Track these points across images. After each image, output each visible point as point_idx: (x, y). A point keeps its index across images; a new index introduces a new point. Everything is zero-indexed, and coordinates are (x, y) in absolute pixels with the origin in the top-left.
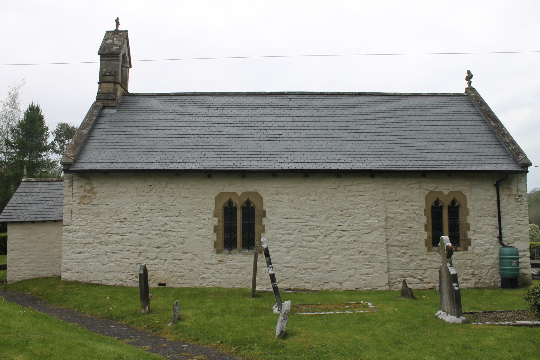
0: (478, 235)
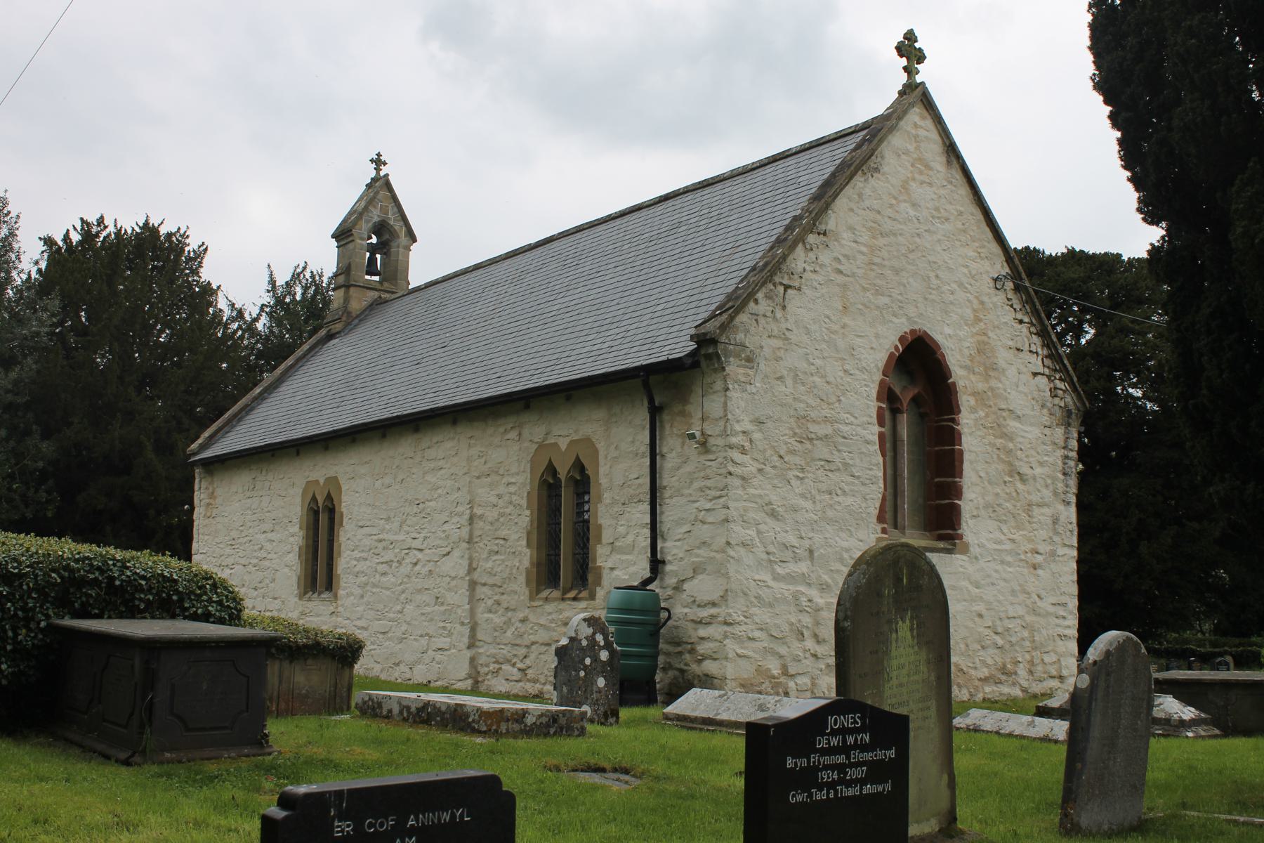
0: (619, 556)
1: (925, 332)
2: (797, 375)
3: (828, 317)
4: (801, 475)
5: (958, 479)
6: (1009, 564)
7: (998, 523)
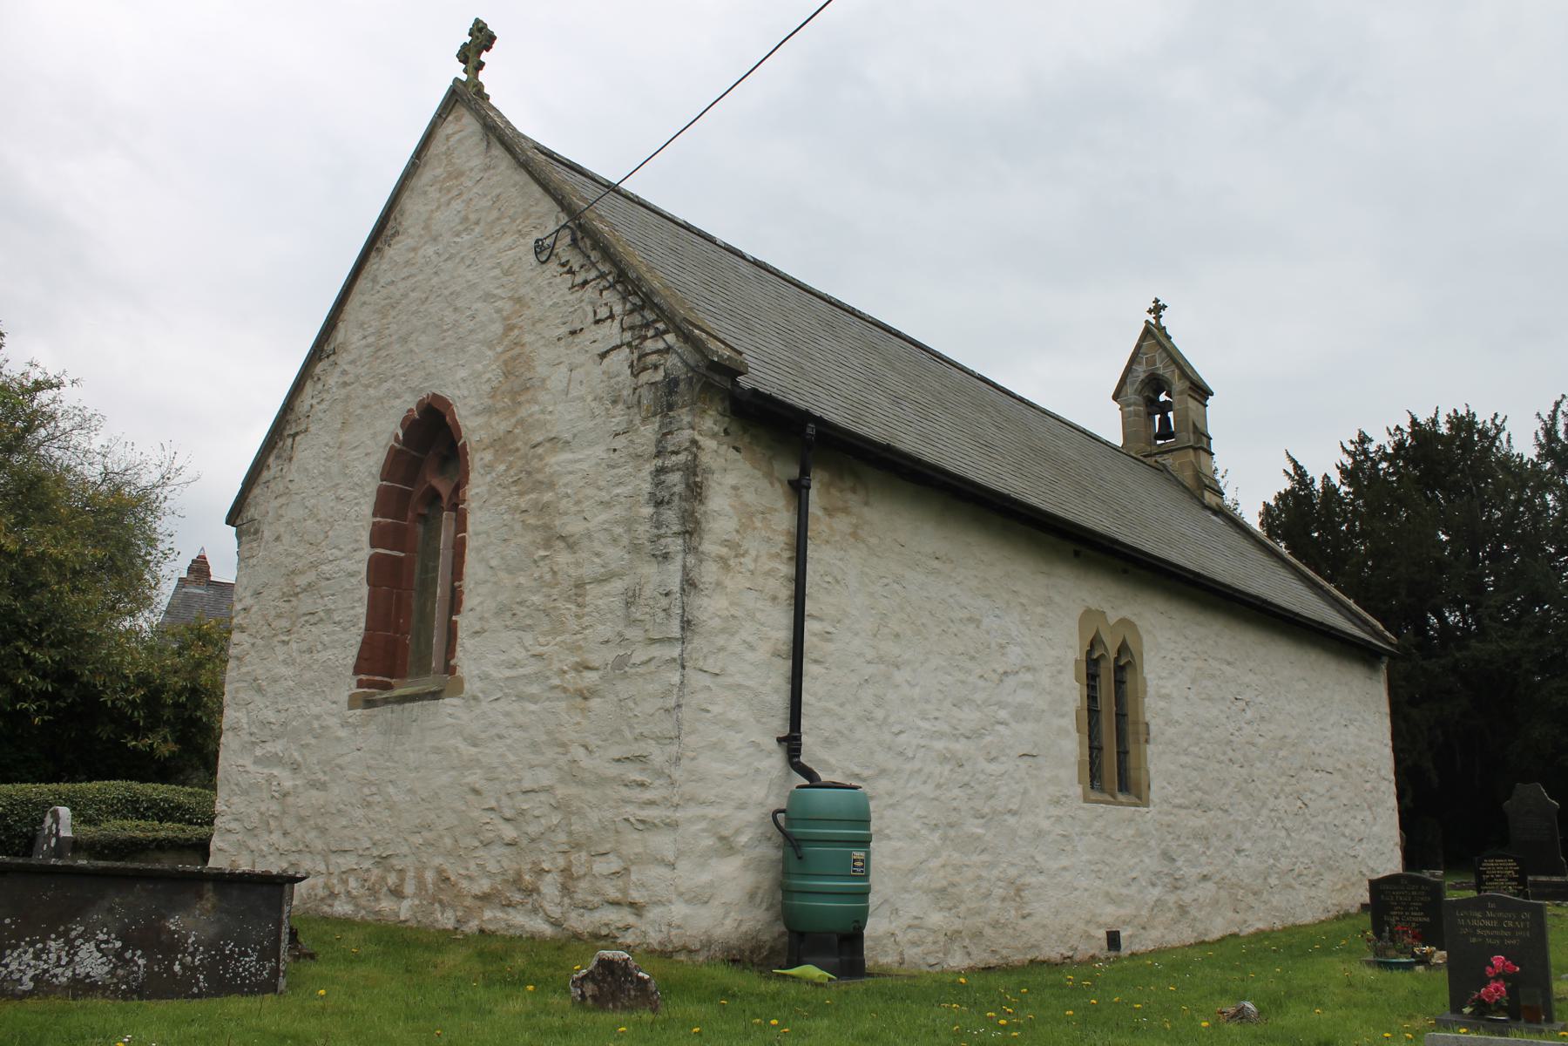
6: (533, 699)
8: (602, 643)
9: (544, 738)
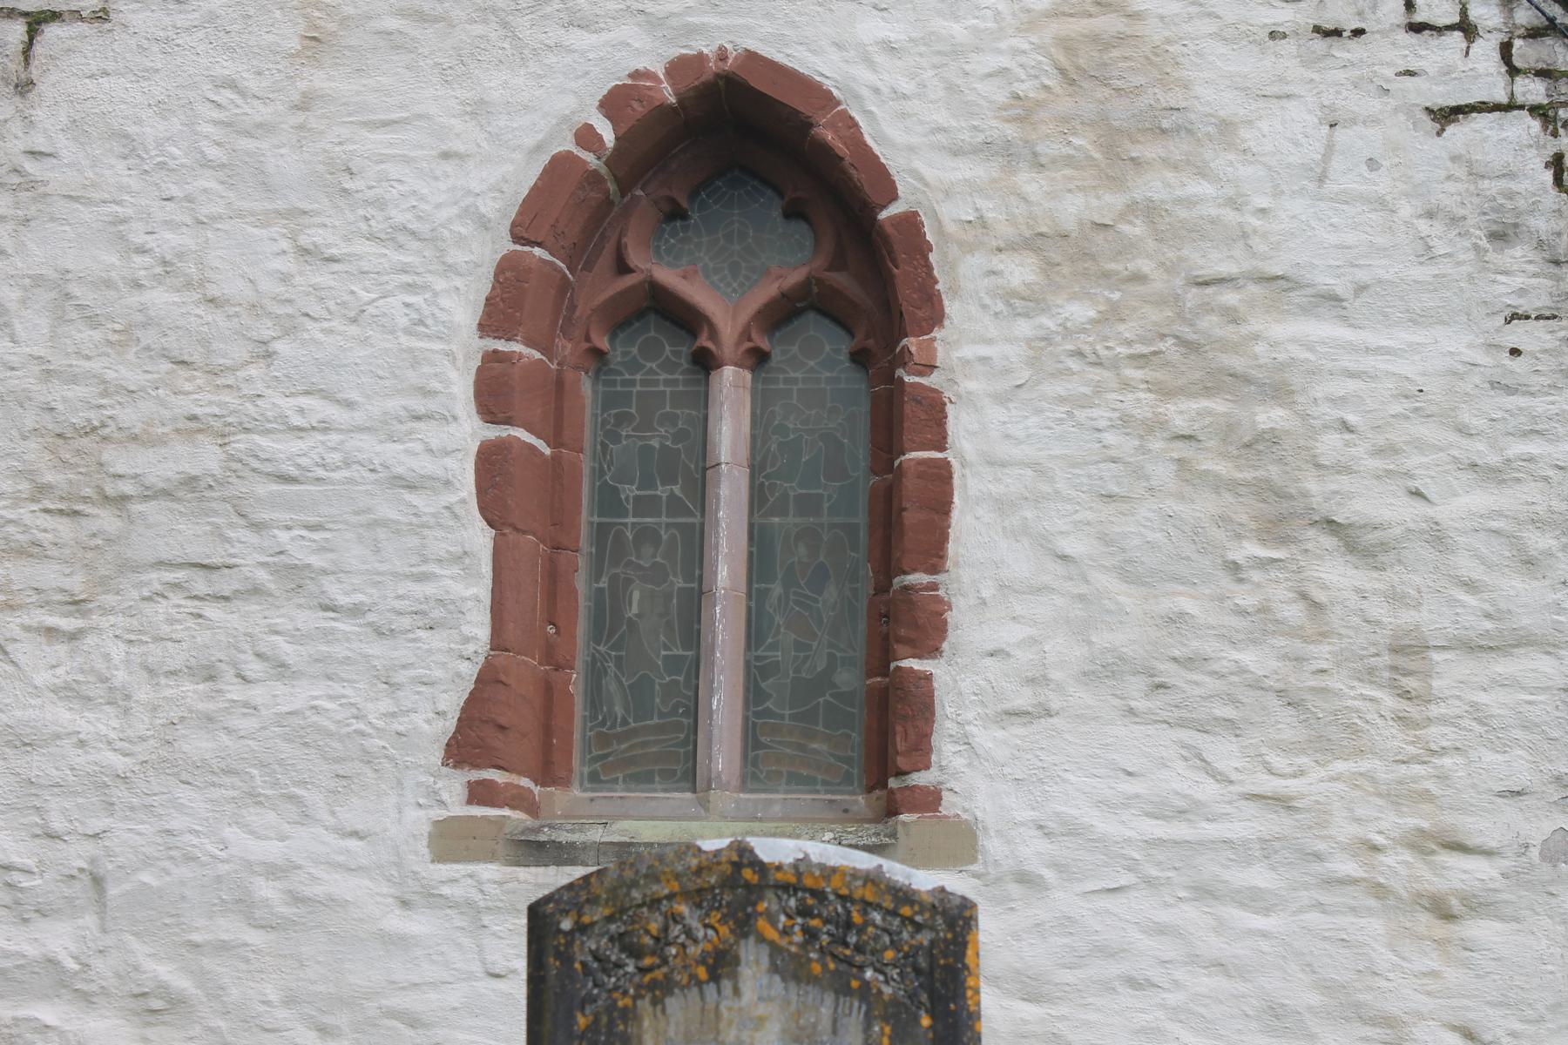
1: (751, 56)
2: (68, 296)
3: (232, 85)
4: (68, 624)
5: (918, 578)
6: (1254, 900)
7: (1187, 735)
8: (1501, 795)
9: (1314, 999)
